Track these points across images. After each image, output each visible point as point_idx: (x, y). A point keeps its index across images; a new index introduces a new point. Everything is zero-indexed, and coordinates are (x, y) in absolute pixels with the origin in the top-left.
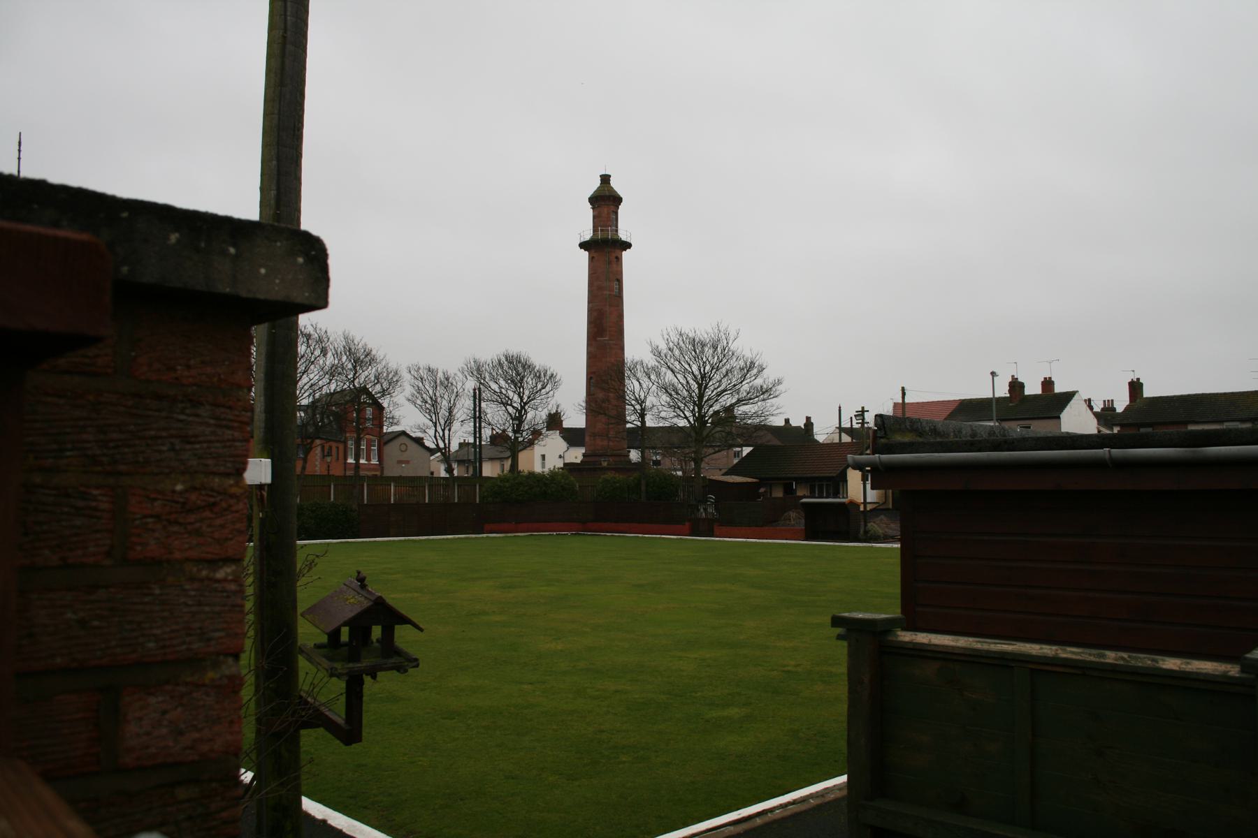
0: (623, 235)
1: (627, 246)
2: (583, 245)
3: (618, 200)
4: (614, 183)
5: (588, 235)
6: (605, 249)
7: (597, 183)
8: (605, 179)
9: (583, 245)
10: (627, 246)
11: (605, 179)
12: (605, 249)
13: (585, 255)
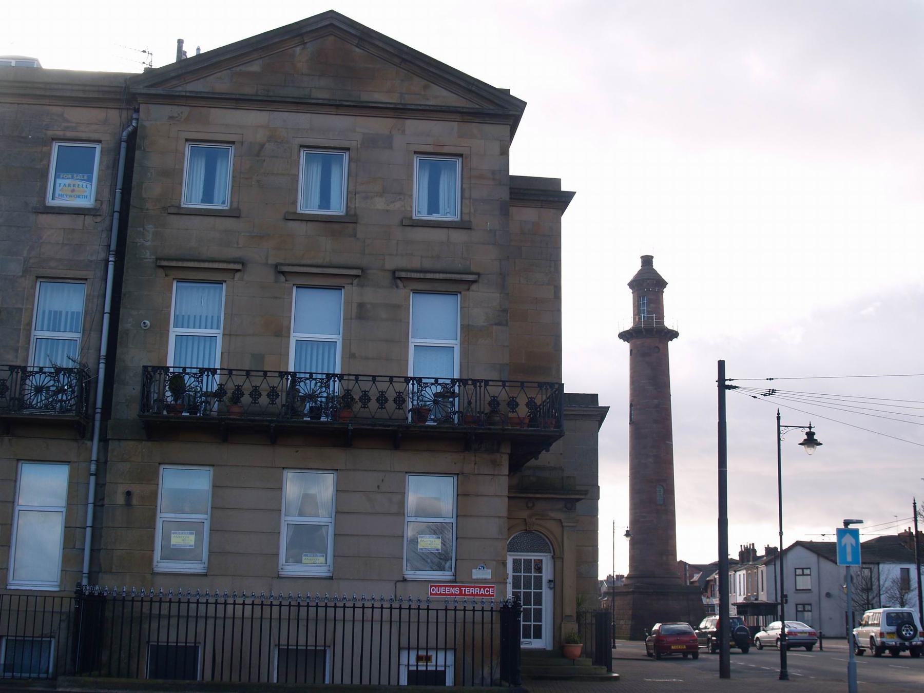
0: (669, 323)
1: (674, 335)
2: (624, 336)
3: (662, 284)
4: (657, 266)
5: (628, 324)
6: (779, 418)
7: (637, 266)
8: (647, 261)
9: (624, 336)
10: (674, 335)
11: (647, 261)
12: (779, 418)
13: (626, 346)
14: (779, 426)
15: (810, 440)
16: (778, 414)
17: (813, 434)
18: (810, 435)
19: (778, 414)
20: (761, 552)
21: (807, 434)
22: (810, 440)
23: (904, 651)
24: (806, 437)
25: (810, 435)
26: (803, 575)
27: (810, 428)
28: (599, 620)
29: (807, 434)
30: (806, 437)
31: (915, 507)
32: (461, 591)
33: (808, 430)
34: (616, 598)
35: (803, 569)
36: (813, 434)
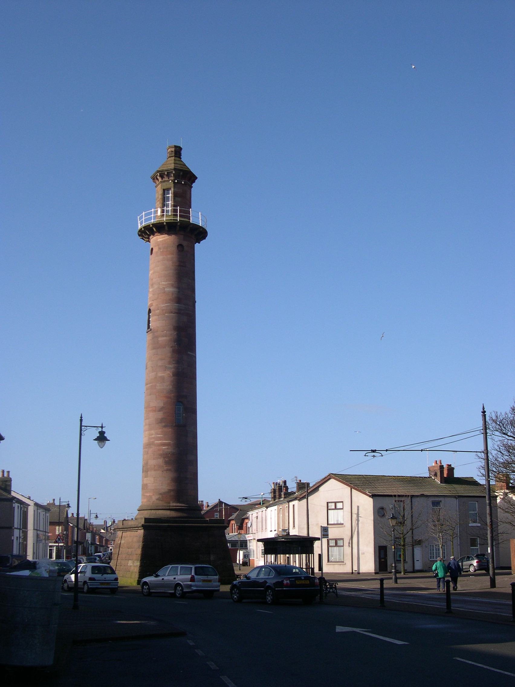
4: (185, 158)
6: (81, 420)
12: (81, 420)
14: (81, 426)
15: (102, 438)
16: (81, 417)
17: (104, 433)
18: (102, 433)
19: (81, 417)
20: (292, 487)
21: (100, 432)
22: (102, 438)
23: (287, 583)
24: (98, 435)
25: (102, 433)
26: (336, 508)
27: (102, 427)
28: (253, 591)
29: (100, 432)
30: (98, 435)
31: (484, 416)
32: (336, 543)
33: (100, 429)
34: (338, 545)
35: (335, 503)
36: (104, 433)
